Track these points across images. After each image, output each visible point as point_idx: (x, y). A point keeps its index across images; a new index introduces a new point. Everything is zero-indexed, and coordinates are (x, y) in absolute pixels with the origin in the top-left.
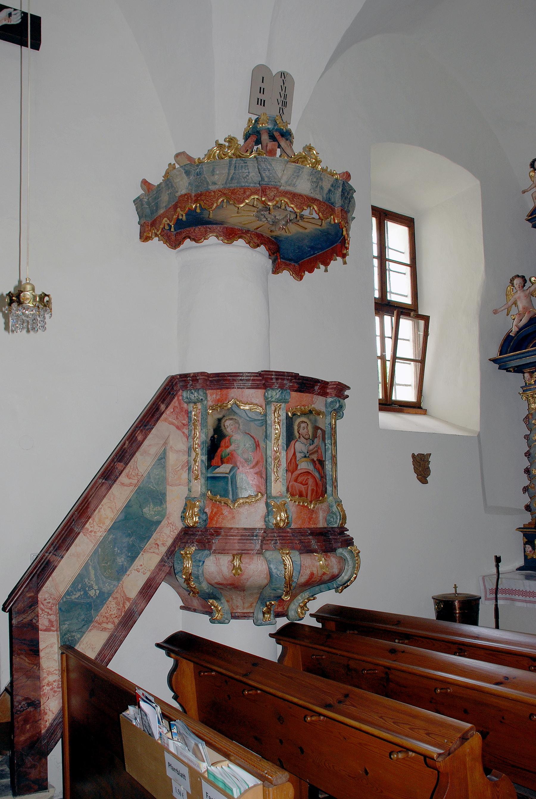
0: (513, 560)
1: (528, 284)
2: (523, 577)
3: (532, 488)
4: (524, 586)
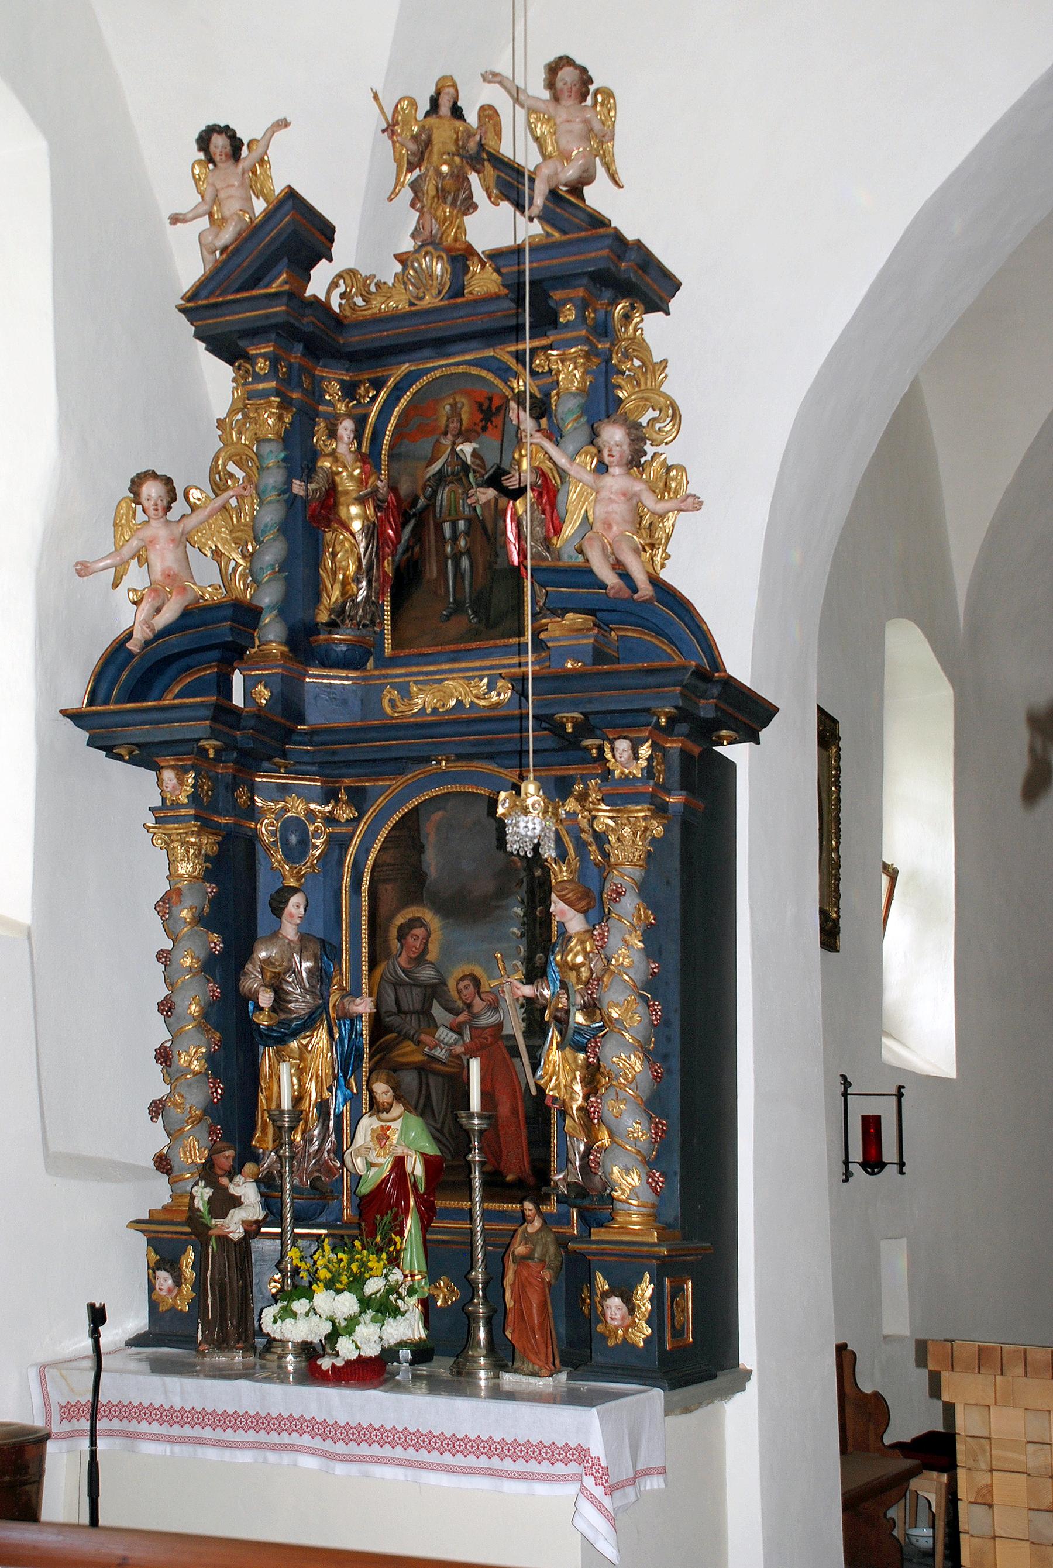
0: (128, 1321)
1: (179, 507)
2: (145, 1366)
3: (177, 1105)
4: (166, 1393)
